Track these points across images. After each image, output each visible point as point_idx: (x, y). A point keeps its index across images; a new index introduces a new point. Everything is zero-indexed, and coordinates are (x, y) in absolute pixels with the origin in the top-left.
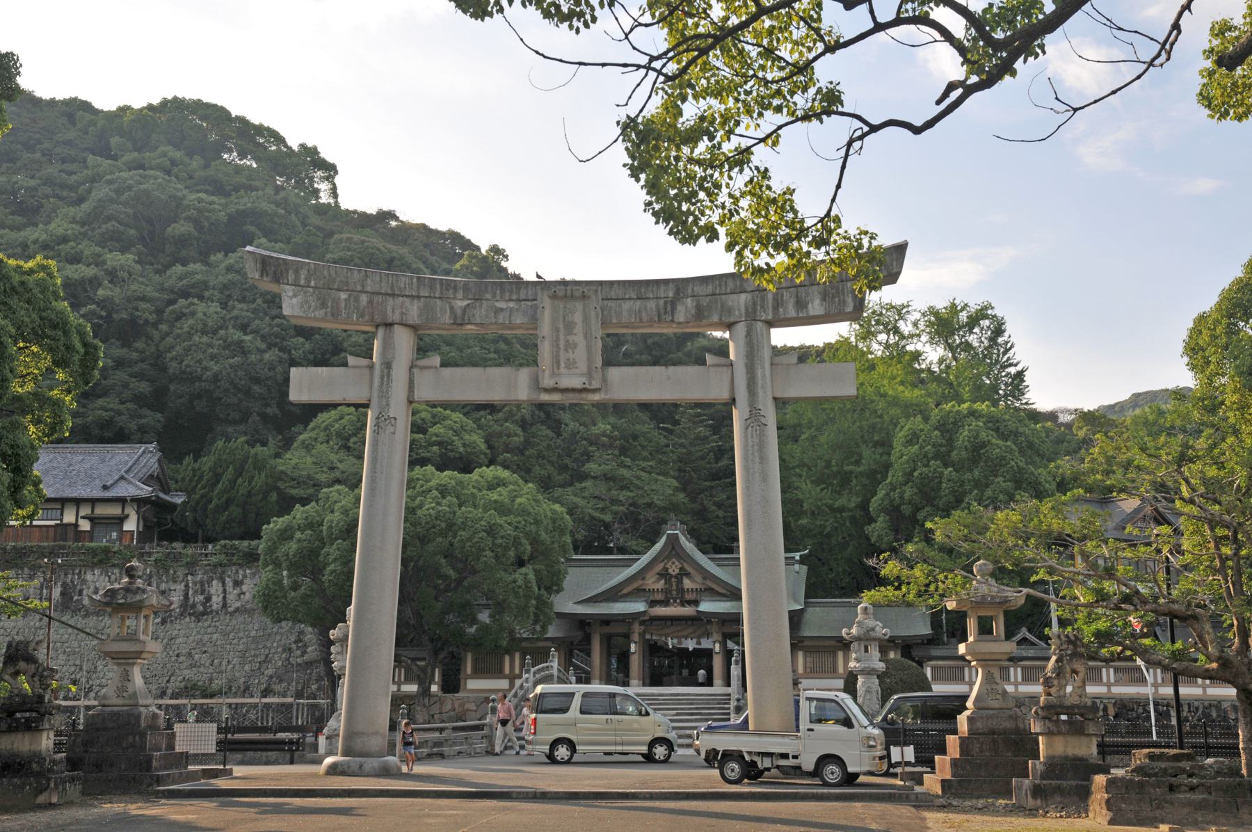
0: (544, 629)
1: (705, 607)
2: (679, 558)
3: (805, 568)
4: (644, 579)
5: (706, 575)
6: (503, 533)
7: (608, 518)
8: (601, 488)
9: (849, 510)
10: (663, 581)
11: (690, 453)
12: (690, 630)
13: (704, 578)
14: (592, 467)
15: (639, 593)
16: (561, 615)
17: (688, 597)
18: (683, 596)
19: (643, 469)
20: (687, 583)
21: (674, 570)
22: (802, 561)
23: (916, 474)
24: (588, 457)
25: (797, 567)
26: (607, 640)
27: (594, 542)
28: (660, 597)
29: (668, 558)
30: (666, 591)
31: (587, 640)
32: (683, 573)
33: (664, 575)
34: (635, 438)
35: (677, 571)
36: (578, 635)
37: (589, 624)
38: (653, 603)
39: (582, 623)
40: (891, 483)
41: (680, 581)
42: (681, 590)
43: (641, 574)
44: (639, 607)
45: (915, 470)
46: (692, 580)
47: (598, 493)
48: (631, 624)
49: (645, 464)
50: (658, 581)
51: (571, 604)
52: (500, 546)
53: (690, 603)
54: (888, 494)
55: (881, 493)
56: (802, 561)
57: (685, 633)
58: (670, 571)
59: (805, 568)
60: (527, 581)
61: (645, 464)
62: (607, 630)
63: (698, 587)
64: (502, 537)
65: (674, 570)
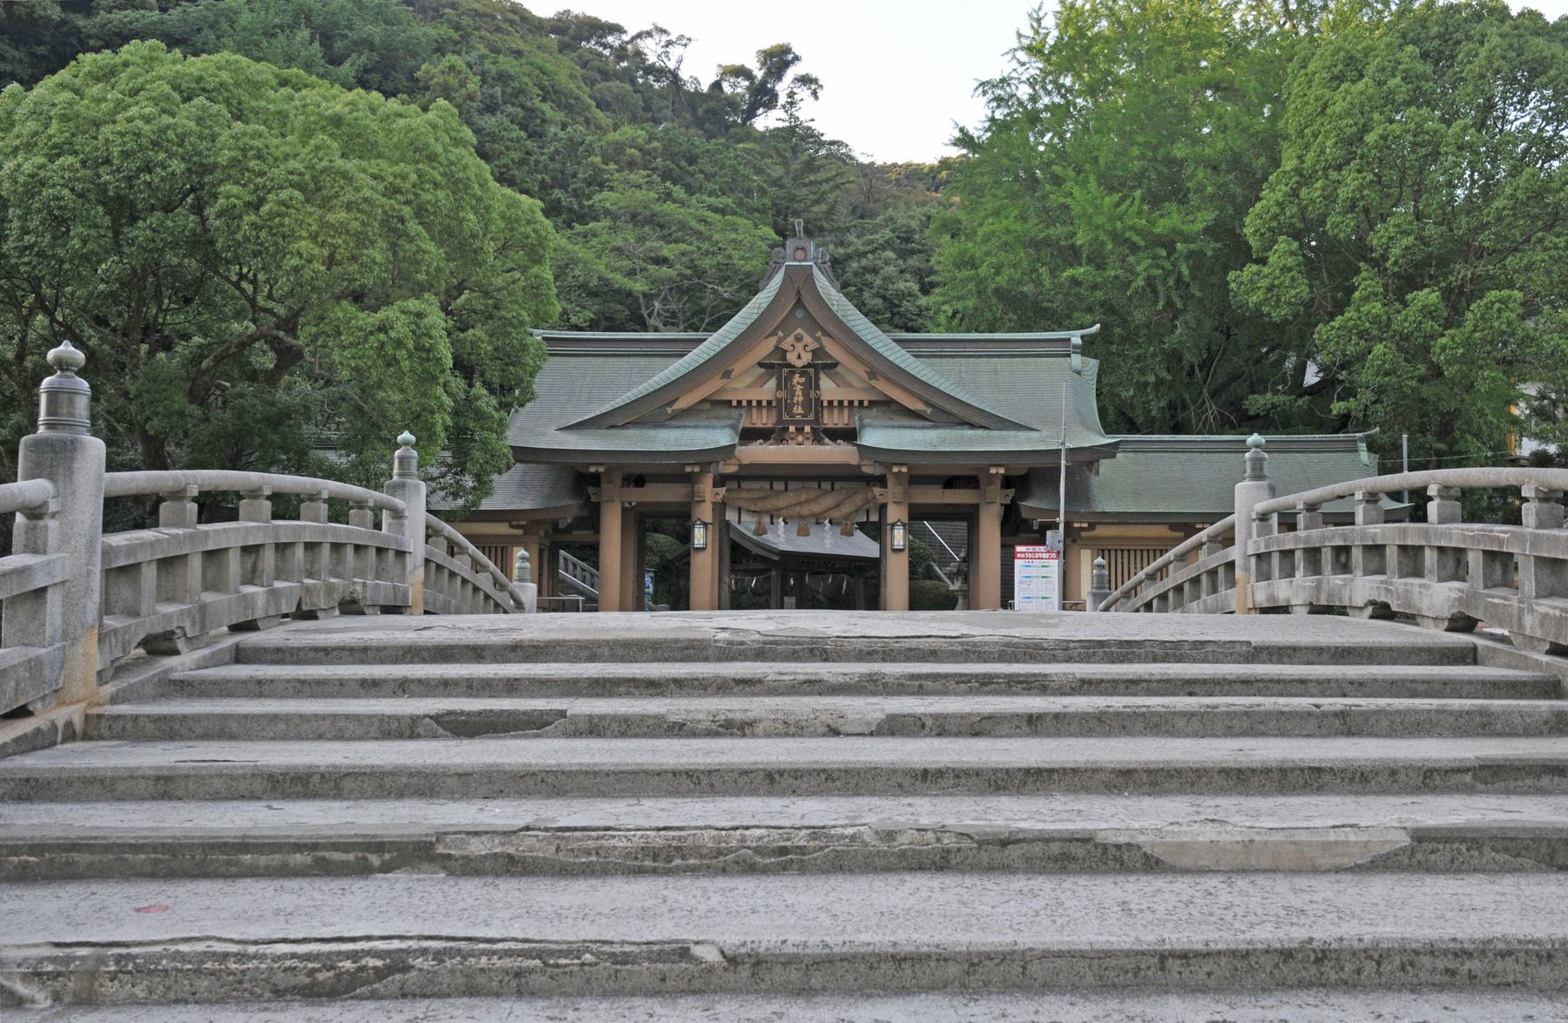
0: (483, 487)
1: (876, 437)
2: (814, 326)
3: (1093, 364)
4: (727, 375)
5: (877, 366)
6: (350, 196)
7: (639, 286)
8: (627, 236)
9: (1187, 239)
10: (772, 383)
11: (793, 199)
12: (828, 501)
13: (873, 374)
14: (605, 199)
15: (717, 405)
16: (524, 455)
17: (832, 420)
18: (817, 419)
19: (711, 208)
20: (829, 389)
21: (799, 356)
22: (1088, 347)
23: (1371, 138)
24: (598, 182)
25: (1076, 360)
26: (641, 522)
27: (616, 313)
28: (763, 420)
29: (786, 326)
30: (779, 407)
31: (592, 519)
32: (822, 365)
33: (776, 366)
34: (692, 160)
35: (807, 358)
36: (569, 508)
37: (596, 480)
38: (748, 435)
39: (582, 479)
40: (1298, 171)
41: (812, 385)
42: (816, 406)
43: (721, 363)
44: (721, 437)
45: (1366, 129)
46: (841, 382)
47: (619, 242)
48: (689, 479)
49: (712, 200)
50: (760, 382)
51: (552, 431)
52: (342, 229)
53: (836, 435)
54: (1295, 193)
55: (1271, 196)
56: (1088, 347)
57: (816, 508)
58: (791, 358)
59: (1093, 364)
60: (420, 333)
61: (712, 200)
62: (637, 496)
63: (856, 397)
64: (349, 207)
65: (799, 356)
